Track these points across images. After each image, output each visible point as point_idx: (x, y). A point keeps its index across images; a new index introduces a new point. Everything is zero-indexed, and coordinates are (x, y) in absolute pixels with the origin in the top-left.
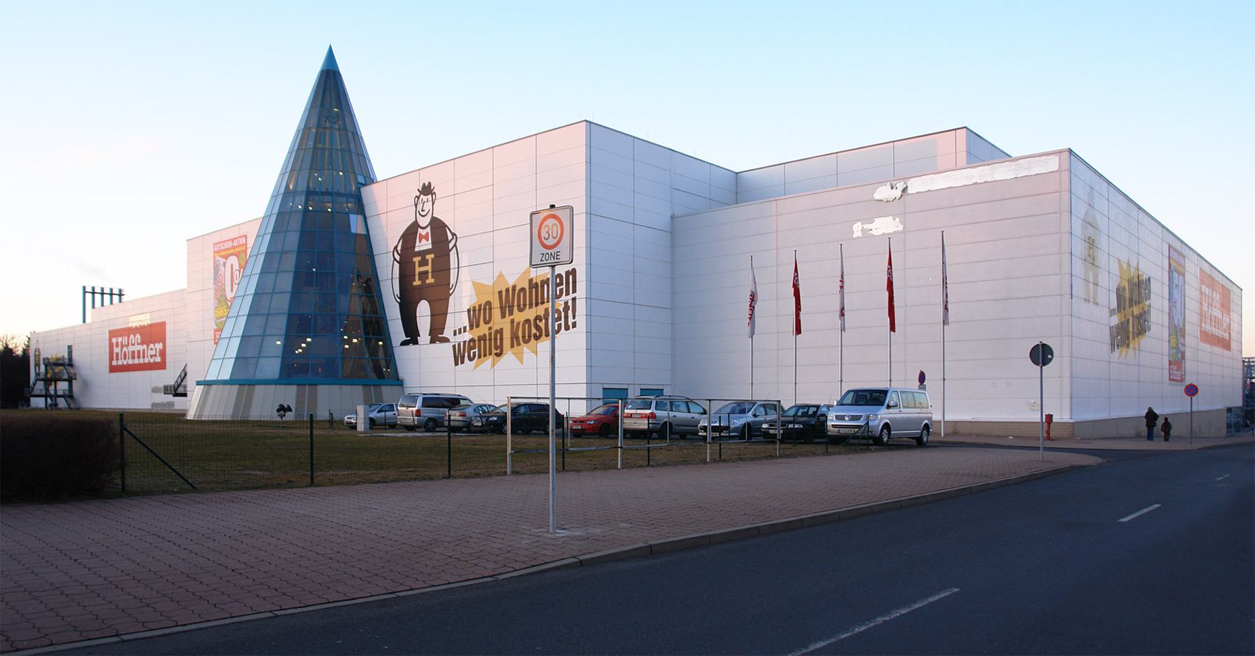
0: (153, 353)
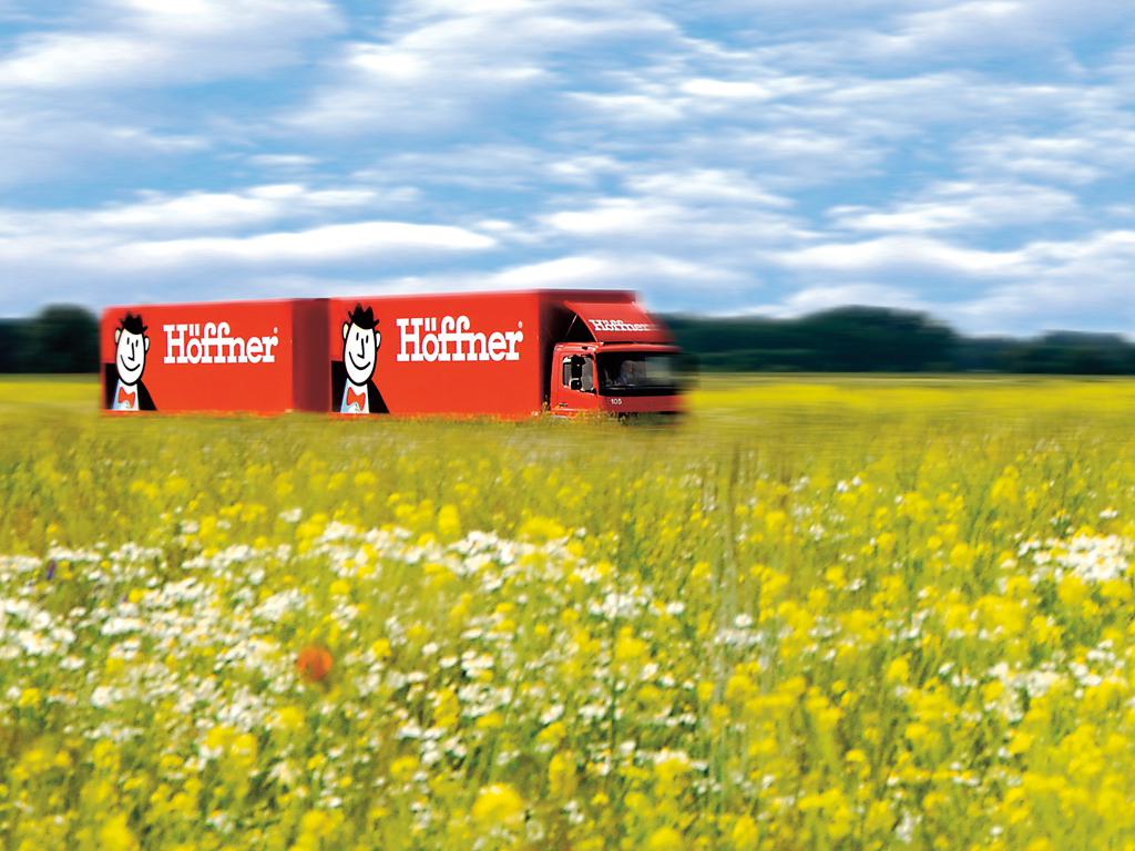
0: (260, 349)
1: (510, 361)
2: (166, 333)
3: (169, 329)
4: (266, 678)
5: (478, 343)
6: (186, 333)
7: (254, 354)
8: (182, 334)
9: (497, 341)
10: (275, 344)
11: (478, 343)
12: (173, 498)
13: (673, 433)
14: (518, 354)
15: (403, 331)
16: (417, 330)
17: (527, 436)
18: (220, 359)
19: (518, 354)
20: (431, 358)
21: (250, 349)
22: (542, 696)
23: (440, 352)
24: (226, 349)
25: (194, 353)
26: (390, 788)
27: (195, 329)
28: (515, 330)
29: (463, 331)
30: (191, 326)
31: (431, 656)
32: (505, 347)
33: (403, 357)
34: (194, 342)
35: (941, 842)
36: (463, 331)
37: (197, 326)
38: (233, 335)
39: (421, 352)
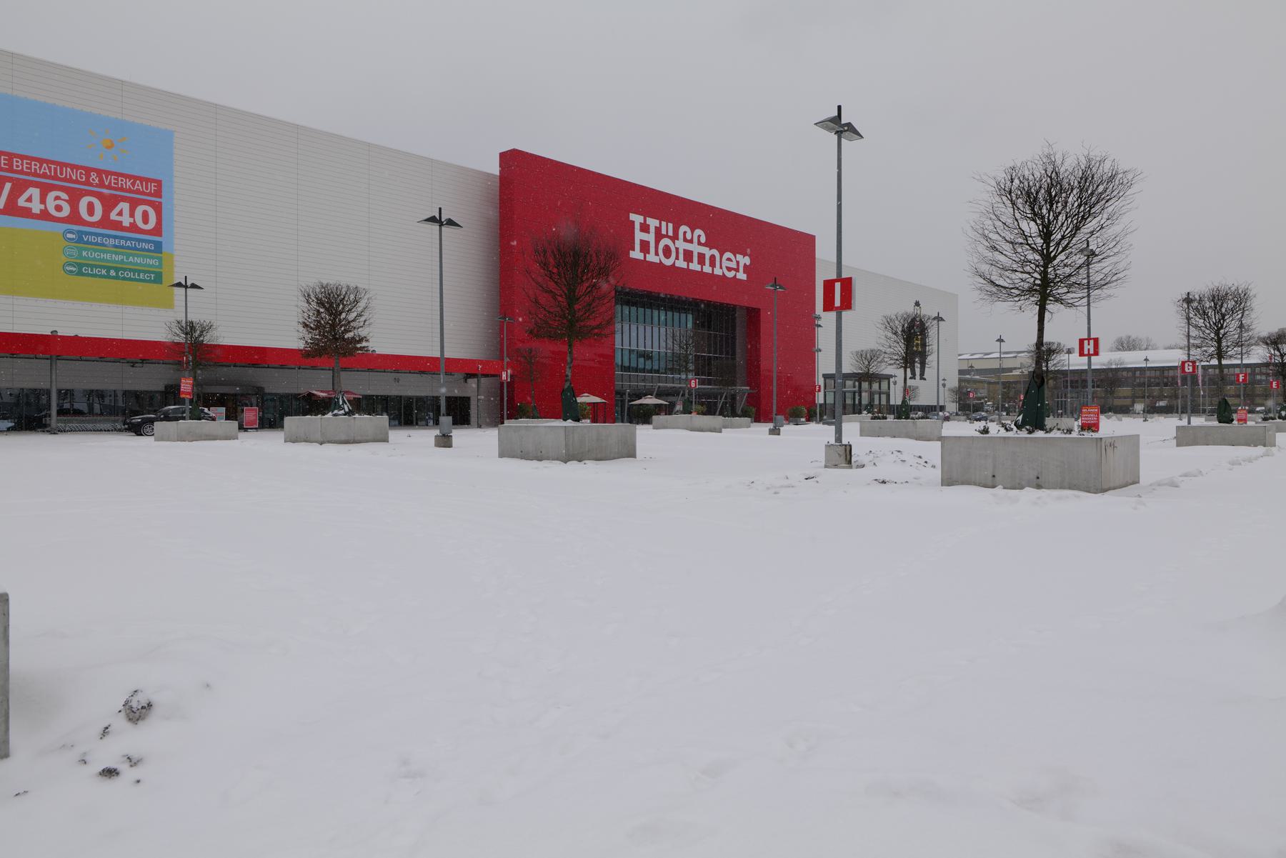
0: (734, 265)
1: (678, 268)
2: (633, 222)
3: (637, 219)
5: (713, 258)
6: (658, 230)
7: (729, 269)
8: (652, 230)
9: (729, 259)
11: (713, 258)
14: (745, 275)
15: (637, 227)
16: (652, 230)
17: (895, 462)
18: (695, 266)
19: (745, 275)
20: (668, 262)
21: (726, 264)
23: (677, 258)
24: (701, 258)
25: (667, 252)
26: (1258, 398)
29: (699, 243)
30: (664, 224)
31: (1220, 372)
32: (735, 267)
33: (636, 254)
35: (1283, 413)
36: (699, 243)
37: (670, 225)
38: (707, 244)
39: (657, 254)
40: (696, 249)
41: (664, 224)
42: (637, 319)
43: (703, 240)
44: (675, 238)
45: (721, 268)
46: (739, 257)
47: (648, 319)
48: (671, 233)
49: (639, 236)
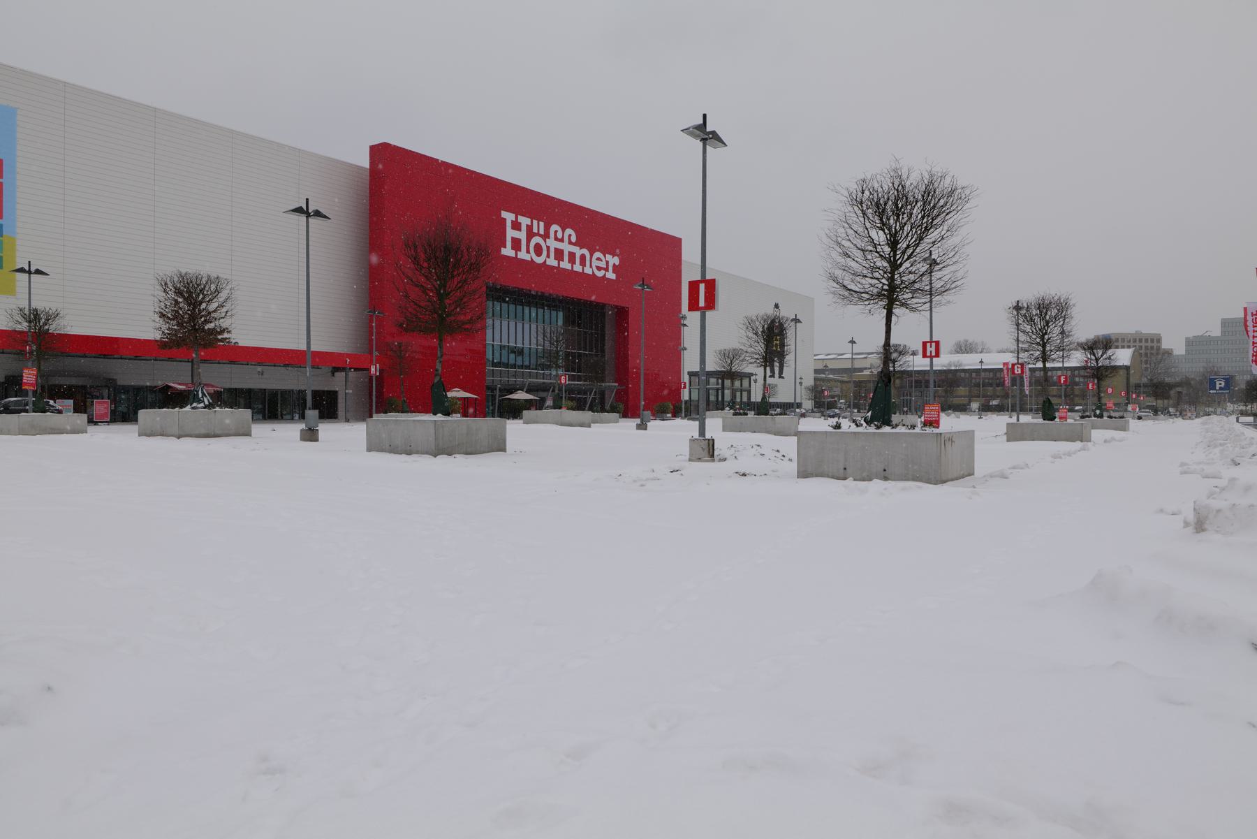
0: (603, 264)
3: (509, 217)
4: (874, 363)
5: (583, 257)
6: (529, 228)
7: (599, 268)
8: (524, 228)
9: (599, 259)
10: (617, 263)
11: (583, 257)
12: (224, 330)
13: (182, 277)
15: (509, 224)
18: (565, 265)
22: (552, 405)
23: (548, 256)
24: (572, 256)
27: (538, 226)
28: (614, 255)
29: (570, 243)
34: (536, 240)
37: (542, 224)
39: (528, 252)
40: (566, 248)
41: (535, 222)
42: (501, 315)
43: (574, 239)
44: (546, 236)
45: (591, 266)
46: (609, 257)
47: (512, 314)
48: (542, 232)
49: (511, 233)
